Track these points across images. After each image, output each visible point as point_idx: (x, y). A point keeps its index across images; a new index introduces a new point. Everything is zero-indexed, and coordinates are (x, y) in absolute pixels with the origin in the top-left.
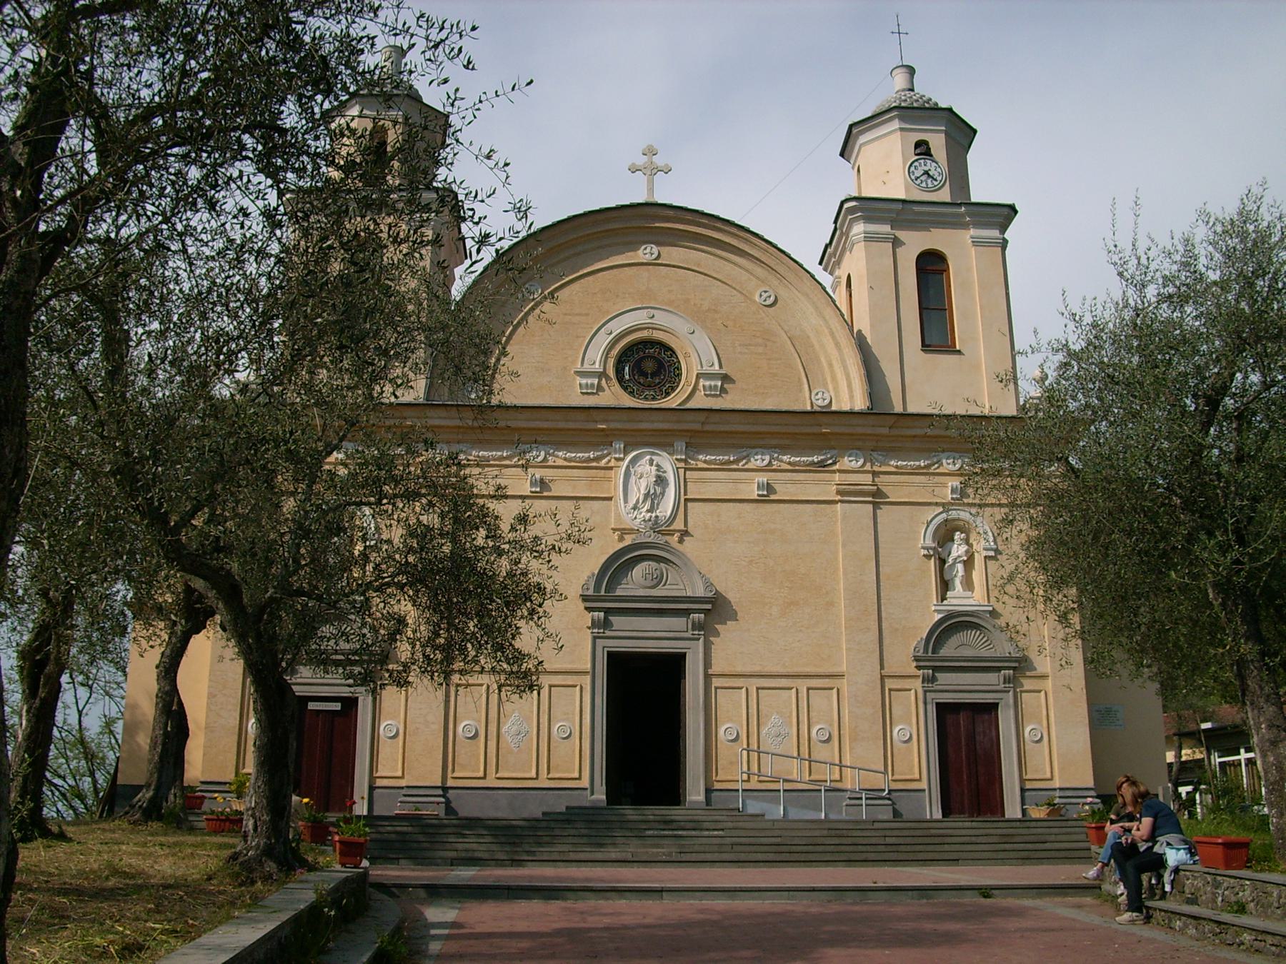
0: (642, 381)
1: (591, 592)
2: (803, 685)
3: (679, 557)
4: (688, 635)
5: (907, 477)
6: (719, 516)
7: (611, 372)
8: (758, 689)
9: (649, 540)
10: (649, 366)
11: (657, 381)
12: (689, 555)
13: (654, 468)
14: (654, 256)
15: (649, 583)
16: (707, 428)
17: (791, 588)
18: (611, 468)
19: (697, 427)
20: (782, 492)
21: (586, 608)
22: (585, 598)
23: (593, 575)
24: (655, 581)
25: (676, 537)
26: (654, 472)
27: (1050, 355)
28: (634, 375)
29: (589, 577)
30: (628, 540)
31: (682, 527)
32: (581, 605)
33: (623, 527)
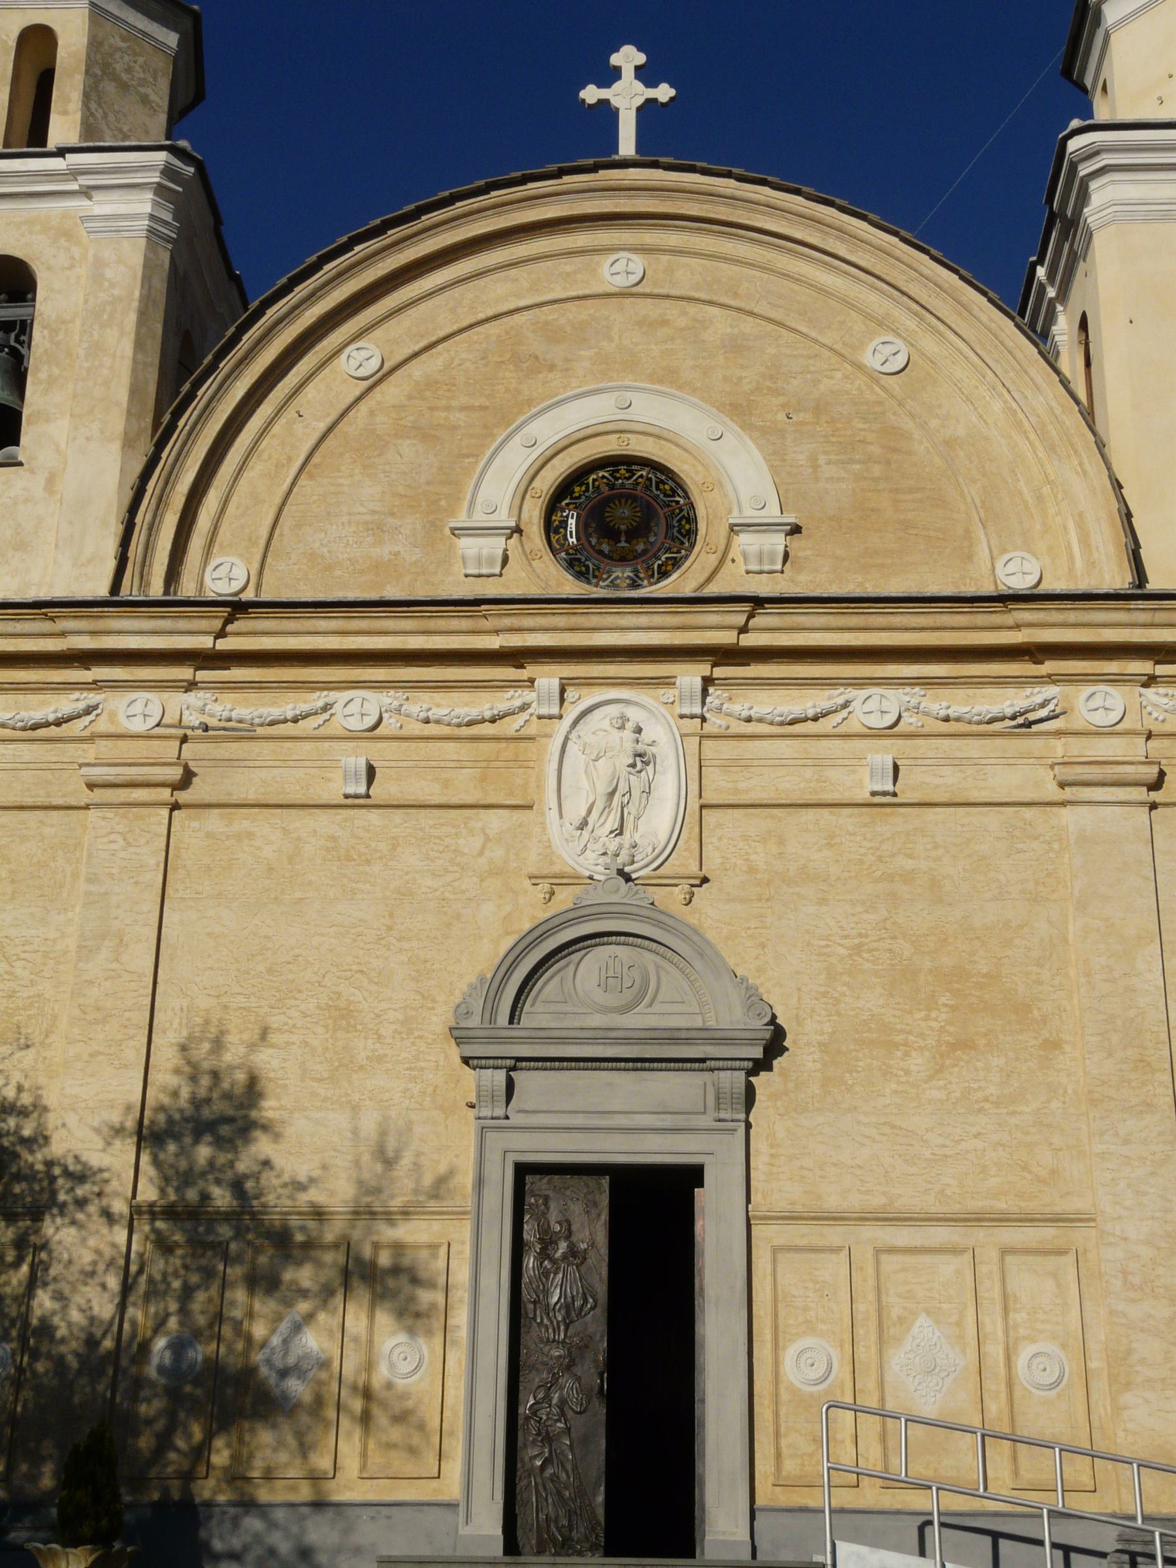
0: (605, 548)
1: (474, 1021)
2: (987, 1240)
3: (685, 938)
4: (706, 1121)
5: (149, 768)
6: (782, 842)
7: (534, 513)
8: (878, 1252)
9: (614, 899)
10: (623, 514)
11: (640, 547)
12: (710, 935)
13: (628, 734)
14: (634, 279)
15: (611, 1000)
16: (747, 640)
17: (954, 1008)
18: (531, 739)
19: (727, 638)
20: (912, 785)
21: (466, 1061)
22: (459, 1036)
23: (482, 980)
24: (628, 995)
25: (679, 893)
26: (629, 746)
27: (621, 734)
28: (588, 536)
29: (472, 987)
30: (565, 898)
31: (694, 868)
32: (455, 1053)
33: (556, 869)
